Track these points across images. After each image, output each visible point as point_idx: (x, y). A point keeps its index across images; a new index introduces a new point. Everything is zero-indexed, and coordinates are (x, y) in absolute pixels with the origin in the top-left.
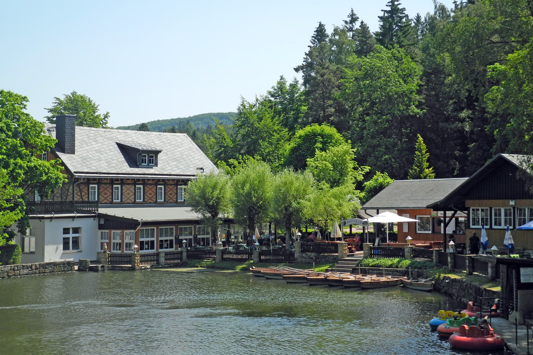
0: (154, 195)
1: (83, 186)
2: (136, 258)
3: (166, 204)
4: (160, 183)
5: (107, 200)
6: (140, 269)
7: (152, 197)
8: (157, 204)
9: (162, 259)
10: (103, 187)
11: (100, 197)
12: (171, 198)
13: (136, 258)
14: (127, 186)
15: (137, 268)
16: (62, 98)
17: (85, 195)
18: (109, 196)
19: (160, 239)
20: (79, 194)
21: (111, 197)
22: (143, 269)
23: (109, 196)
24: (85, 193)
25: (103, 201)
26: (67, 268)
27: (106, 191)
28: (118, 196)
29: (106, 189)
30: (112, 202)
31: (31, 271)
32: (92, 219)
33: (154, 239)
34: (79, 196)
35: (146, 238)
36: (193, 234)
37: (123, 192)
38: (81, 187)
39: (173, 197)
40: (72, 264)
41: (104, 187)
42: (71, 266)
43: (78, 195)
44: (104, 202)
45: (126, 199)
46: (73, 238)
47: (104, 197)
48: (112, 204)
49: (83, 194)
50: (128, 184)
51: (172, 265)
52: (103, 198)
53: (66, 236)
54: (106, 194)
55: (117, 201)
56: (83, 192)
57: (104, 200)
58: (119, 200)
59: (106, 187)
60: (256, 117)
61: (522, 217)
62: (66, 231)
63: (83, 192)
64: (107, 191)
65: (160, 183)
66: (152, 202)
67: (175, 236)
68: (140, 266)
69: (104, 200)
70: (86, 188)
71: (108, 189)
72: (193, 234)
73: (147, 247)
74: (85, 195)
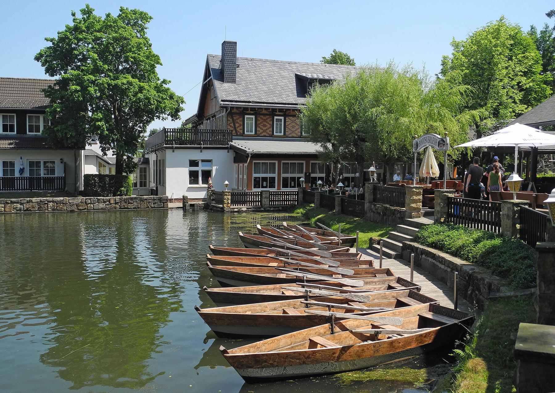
0: (270, 128)
1: (237, 117)
2: (225, 197)
3: (285, 138)
4: (248, 112)
5: (267, 133)
6: (231, 212)
7: (267, 130)
8: (272, 137)
9: (266, 200)
10: (261, 118)
11: (258, 129)
12: (293, 132)
13: (225, 197)
14: (291, 118)
15: (227, 210)
16: (100, 13)
17: (239, 127)
18: (268, 128)
19: (283, 175)
20: (232, 125)
21: (271, 129)
22: (236, 212)
23: (268, 128)
24: (239, 123)
25: (261, 133)
26: (159, 205)
27: (265, 123)
28: (281, 129)
29: (265, 121)
30: (243, 134)
31: (110, 206)
32: (226, 151)
33: (275, 175)
34: (232, 127)
35: (290, 173)
36: (304, 171)
37: (287, 124)
38: (235, 118)
39: (267, 130)
40: (164, 200)
41: (262, 119)
42: (164, 203)
43: (231, 126)
44: (262, 135)
45: (290, 132)
46: (203, 171)
47: (262, 129)
48: (243, 136)
49: (237, 125)
50: (265, 115)
51: (281, 208)
52: (261, 131)
53: (194, 169)
54: (265, 126)
55: (249, 133)
56: (237, 123)
57: (262, 132)
58: (282, 134)
59: (265, 118)
60: (530, 64)
61: (9, 168)
62: (193, 163)
63: (237, 123)
64: (267, 122)
65: (248, 112)
66: (267, 135)
67: (306, 173)
68: (232, 207)
69: (262, 132)
70: (241, 119)
71: (268, 121)
72: (304, 171)
73: (293, 184)
74: (239, 127)
